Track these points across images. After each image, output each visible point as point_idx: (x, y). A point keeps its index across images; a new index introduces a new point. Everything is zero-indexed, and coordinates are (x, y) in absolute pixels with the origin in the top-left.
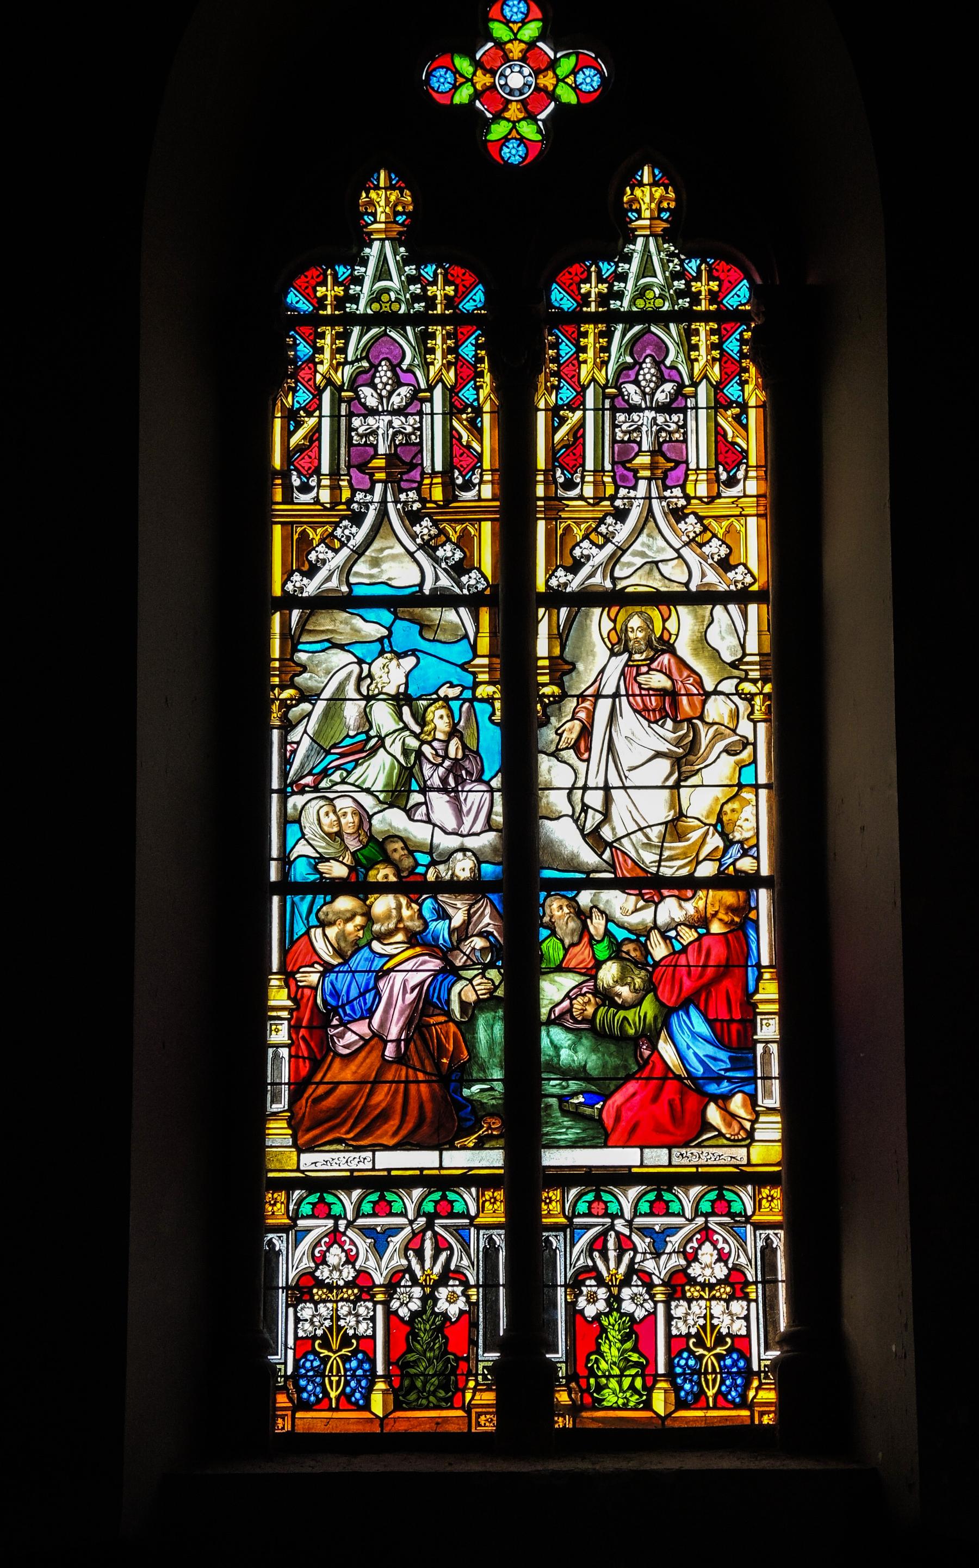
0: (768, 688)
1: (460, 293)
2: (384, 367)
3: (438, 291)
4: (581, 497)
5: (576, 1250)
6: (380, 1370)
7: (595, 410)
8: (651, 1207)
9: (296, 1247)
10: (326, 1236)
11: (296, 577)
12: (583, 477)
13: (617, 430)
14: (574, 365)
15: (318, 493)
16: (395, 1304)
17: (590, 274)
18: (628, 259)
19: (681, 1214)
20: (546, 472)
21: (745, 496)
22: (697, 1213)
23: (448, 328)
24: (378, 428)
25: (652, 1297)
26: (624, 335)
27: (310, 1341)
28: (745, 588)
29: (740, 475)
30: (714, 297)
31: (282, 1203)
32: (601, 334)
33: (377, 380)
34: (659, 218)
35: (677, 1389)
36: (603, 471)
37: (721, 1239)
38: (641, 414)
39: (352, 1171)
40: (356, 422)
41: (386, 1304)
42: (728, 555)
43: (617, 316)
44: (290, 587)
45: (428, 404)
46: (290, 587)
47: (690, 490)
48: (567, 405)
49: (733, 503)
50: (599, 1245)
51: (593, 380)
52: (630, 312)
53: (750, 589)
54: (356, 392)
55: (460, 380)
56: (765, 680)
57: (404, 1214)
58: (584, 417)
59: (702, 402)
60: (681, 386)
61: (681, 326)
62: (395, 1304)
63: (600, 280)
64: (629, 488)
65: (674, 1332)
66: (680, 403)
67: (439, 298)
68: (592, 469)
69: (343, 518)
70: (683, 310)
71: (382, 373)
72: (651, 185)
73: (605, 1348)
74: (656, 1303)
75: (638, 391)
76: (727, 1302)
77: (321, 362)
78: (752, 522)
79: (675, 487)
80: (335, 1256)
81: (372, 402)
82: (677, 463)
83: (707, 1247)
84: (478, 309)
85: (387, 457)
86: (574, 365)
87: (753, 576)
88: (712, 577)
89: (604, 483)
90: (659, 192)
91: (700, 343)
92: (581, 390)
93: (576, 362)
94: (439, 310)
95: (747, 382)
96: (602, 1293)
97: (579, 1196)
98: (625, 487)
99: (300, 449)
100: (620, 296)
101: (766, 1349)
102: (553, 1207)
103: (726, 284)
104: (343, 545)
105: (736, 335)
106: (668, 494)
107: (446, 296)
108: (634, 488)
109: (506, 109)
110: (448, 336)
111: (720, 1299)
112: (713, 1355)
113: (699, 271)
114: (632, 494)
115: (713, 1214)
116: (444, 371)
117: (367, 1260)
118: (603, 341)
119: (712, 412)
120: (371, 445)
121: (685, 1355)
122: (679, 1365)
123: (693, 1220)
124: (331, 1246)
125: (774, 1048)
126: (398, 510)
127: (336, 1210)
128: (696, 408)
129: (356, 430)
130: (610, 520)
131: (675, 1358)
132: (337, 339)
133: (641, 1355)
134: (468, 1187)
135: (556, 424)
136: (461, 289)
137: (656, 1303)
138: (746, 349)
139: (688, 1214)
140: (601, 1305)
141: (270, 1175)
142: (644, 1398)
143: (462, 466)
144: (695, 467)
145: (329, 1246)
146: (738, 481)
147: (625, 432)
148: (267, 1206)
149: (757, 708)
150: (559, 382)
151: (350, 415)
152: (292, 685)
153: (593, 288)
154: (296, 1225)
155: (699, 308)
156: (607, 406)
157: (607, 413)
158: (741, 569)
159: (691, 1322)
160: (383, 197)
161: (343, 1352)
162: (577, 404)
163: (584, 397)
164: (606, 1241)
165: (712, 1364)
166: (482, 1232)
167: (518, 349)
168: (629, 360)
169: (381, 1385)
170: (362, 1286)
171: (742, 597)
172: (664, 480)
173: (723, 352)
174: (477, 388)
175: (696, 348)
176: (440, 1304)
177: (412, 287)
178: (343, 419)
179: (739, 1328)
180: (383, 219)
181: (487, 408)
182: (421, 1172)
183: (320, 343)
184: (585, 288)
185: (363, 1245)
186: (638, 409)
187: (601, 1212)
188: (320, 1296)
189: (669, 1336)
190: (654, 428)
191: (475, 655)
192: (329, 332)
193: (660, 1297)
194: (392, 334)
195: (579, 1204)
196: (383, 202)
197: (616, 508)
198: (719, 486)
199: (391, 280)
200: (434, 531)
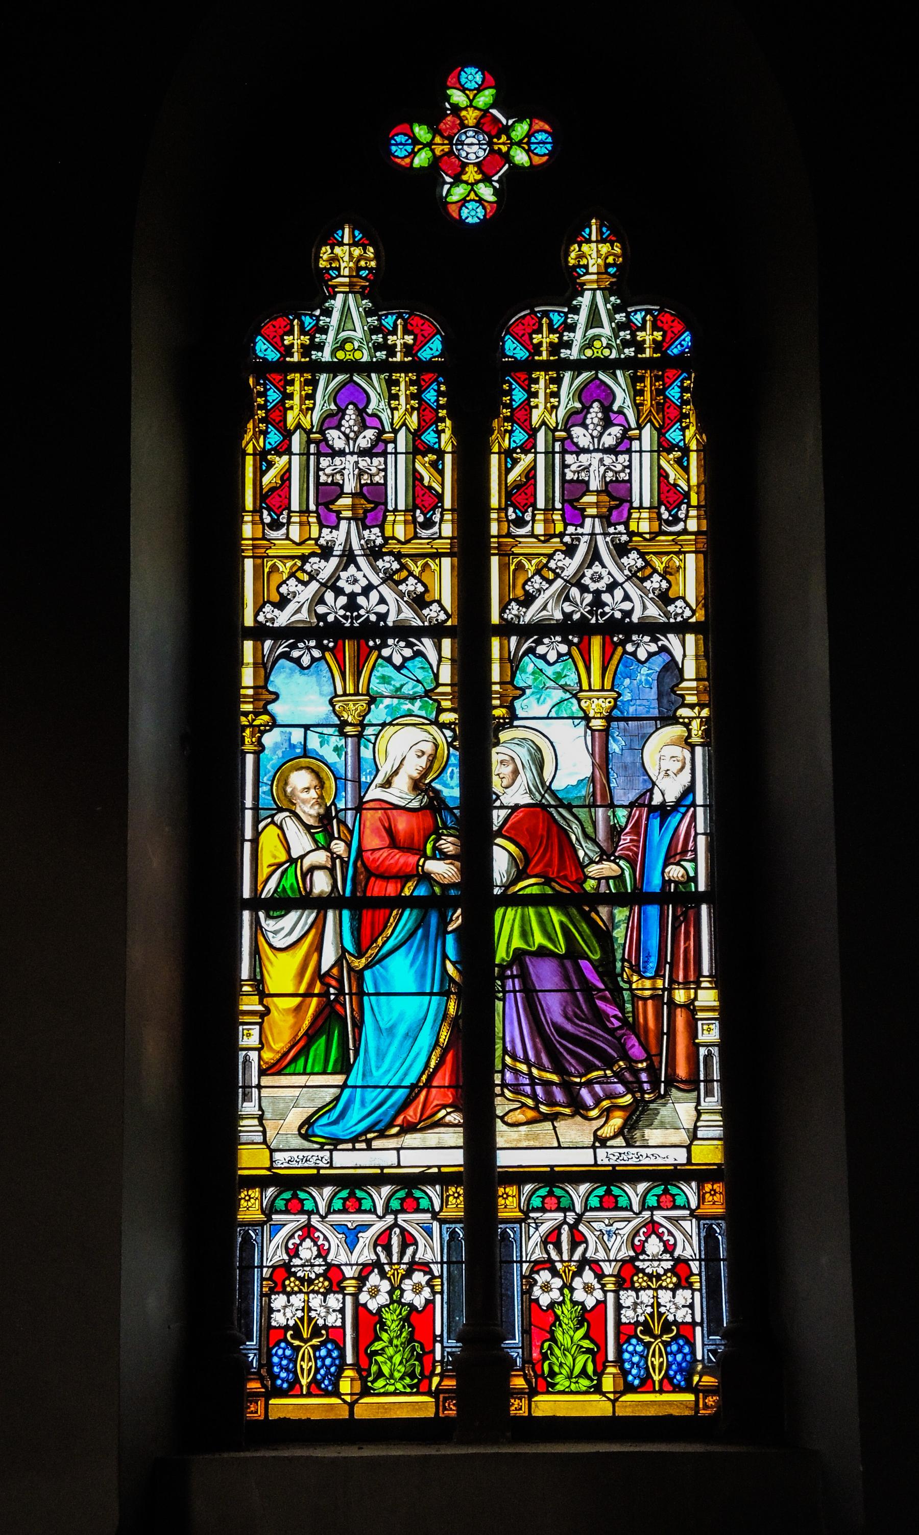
0: (705, 713)
1: (667, 340)
2: (351, 410)
3: (398, 340)
4: (533, 535)
5: (531, 1243)
6: (349, 1359)
7: (546, 453)
8: (601, 1202)
9: (270, 1241)
10: (644, 1226)
11: (268, 608)
12: (534, 516)
13: (321, 473)
14: (526, 410)
15: (533, 527)
16: (364, 1298)
17: (541, 325)
18: (576, 310)
19: (373, 1211)
20: (499, 510)
21: (440, 537)
22: (644, 1207)
23: (410, 375)
26: (573, 380)
27: (283, 1331)
28: (685, 621)
29: (437, 518)
30: (408, 350)
31: (721, 1193)
32: (307, 383)
33: (588, 421)
34: (358, 276)
35: (625, 1373)
36: (554, 509)
37: (322, 1237)
38: (343, 459)
39: (614, 1166)
40: (570, 459)
41: (355, 1296)
42: (668, 589)
43: (318, 367)
44: (261, 618)
45: (637, 442)
46: (261, 618)
47: (633, 526)
48: (520, 447)
49: (428, 544)
51: (544, 423)
52: (579, 361)
53: (690, 621)
54: (324, 435)
55: (423, 424)
56: (702, 706)
57: (373, 1211)
58: (535, 460)
59: (401, 447)
60: (382, 431)
61: (382, 376)
62: (364, 1298)
63: (303, 332)
64: (576, 526)
65: (624, 1320)
66: (381, 446)
67: (648, 342)
68: (404, 508)
69: (313, 554)
70: (628, 358)
71: (593, 415)
72: (350, 245)
73: (559, 1334)
75: (342, 436)
76: (325, 1295)
77: (291, 408)
78: (691, 559)
79: (619, 524)
80: (654, 1246)
81: (339, 444)
82: (377, 504)
83: (654, 1239)
84: (435, 357)
85: (353, 495)
86: (526, 410)
87: (446, 612)
88: (408, 613)
90: (605, 248)
91: (400, 393)
92: (288, 435)
93: (527, 407)
94: (648, 353)
96: (385, 1286)
97: (533, 1192)
98: (573, 525)
99: (518, 486)
100: (320, 347)
101: (449, 1338)
102: (509, 1203)
103: (670, 335)
104: (557, 576)
105: (678, 383)
106: (611, 530)
107: (405, 345)
108: (582, 526)
109: (463, 172)
110: (307, 383)
112: (311, 1346)
113: (644, 321)
114: (580, 530)
115: (659, 1208)
116: (407, 416)
117: (338, 1254)
118: (554, 388)
120: (338, 484)
121: (283, 1345)
122: (276, 1354)
123: (640, 1213)
124: (649, 1236)
125: (715, 1051)
126: (607, 542)
127: (309, 1205)
128: (396, 453)
129: (323, 470)
130: (559, 556)
131: (273, 1348)
132: (550, 383)
133: (592, 1341)
134: (433, 1185)
135: (264, 468)
137: (434, 1293)
138: (687, 396)
139: (636, 1208)
140: (555, 1295)
141: (240, 1172)
142: (595, 1382)
143: (668, 502)
144: (638, 505)
145: (302, 1239)
146: (434, 523)
148: (242, 1201)
149: (694, 732)
150: (512, 426)
151: (564, 452)
152: (266, 712)
153: (544, 339)
154: (271, 1220)
155: (395, 359)
156: (557, 449)
158: (435, 607)
159: (289, 1315)
160: (595, 250)
161: (665, 1338)
163: (535, 439)
164: (560, 1234)
165: (659, 1348)
166: (445, 1227)
167: (474, 395)
168: (578, 405)
169: (349, 1373)
170: (333, 1278)
171: (436, 632)
172: (363, 520)
173: (421, 401)
174: (439, 433)
175: (396, 397)
176: (406, 1294)
177: (622, 334)
178: (557, 456)
179: (333, 1320)
180: (346, 272)
181: (693, 446)
182: (382, 1171)
183: (534, 388)
184: (537, 338)
185: (335, 1241)
186: (342, 453)
187: (670, 1205)
188: (292, 1289)
189: (618, 1323)
191: (438, 685)
192: (542, 376)
196: (346, 255)
197: (565, 544)
198: (415, 528)
199: (603, 327)
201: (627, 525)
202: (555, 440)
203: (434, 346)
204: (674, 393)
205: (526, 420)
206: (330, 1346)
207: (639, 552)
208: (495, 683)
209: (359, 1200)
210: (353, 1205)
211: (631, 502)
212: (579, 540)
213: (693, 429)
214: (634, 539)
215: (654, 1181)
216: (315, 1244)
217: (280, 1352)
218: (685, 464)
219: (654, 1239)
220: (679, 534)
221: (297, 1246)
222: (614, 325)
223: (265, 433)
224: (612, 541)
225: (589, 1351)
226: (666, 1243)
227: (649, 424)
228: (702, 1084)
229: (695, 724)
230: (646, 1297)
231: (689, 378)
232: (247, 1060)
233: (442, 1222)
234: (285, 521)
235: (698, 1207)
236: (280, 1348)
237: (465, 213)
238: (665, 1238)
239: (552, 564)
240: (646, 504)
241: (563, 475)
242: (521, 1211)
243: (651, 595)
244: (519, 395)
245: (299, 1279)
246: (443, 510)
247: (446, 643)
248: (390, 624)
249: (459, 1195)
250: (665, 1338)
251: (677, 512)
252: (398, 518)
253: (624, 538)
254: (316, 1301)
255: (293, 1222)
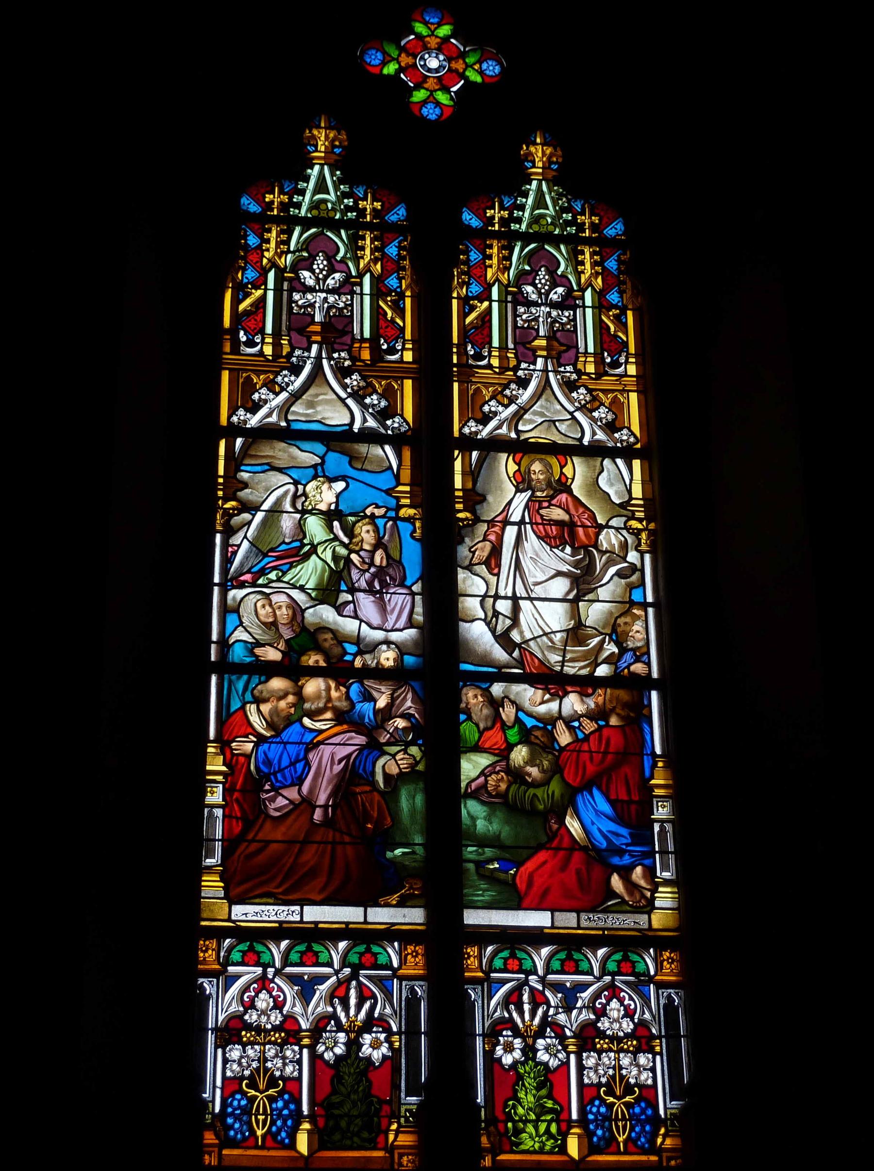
0: (652, 526)
4: (489, 366)
11: (241, 412)
15: (626, 368)
16: (321, 1048)
18: (526, 195)
19: (590, 972)
21: (626, 375)
22: (604, 972)
24: (315, 302)
25: (565, 1048)
29: (622, 360)
30: (594, 227)
32: (503, 248)
33: (537, 281)
36: (507, 348)
37: (627, 997)
40: (296, 296)
44: (235, 419)
47: (580, 366)
49: (616, 380)
50: (514, 998)
51: (497, 280)
52: (526, 233)
57: (590, 972)
64: (529, 363)
65: (586, 1081)
70: (569, 234)
73: (521, 1095)
74: (568, 1054)
80: (263, 1001)
81: (310, 282)
82: (569, 348)
83: (614, 1004)
87: (635, 437)
88: (601, 436)
89: (508, 358)
92: (264, 272)
95: (625, 292)
97: (494, 954)
100: (519, 221)
102: (474, 960)
107: (374, 210)
108: (535, 363)
111: (627, 1051)
115: (619, 973)
117: (293, 1005)
119: (597, 311)
120: (309, 314)
121: (597, 1103)
122: (591, 1112)
125: (668, 827)
126: (558, 379)
129: (297, 302)
133: (556, 1102)
135: (241, 297)
136: (387, 205)
139: (596, 972)
140: (517, 1054)
147: (525, 321)
149: (643, 541)
150: (469, 279)
154: (226, 971)
156: (285, 287)
157: (509, 305)
160: (540, 151)
161: (627, 1099)
162: (485, 296)
164: (348, 990)
165: (622, 1111)
170: (289, 1032)
173: (384, 255)
175: (582, 263)
185: (289, 991)
187: (516, 968)
188: (629, 1047)
190: (326, 305)
193: (572, 1048)
194: (329, 234)
195: (350, 955)
199: (329, 193)
200: (362, 384)
201: (575, 365)
202: (508, 293)
203: (400, 213)
204: (392, 250)
205: (481, 276)
206: (286, 1097)
207: (587, 388)
208: (221, 477)
209: (577, 962)
210: (571, 966)
211: (578, 349)
212: (305, 362)
213: (629, 293)
214: (583, 377)
215: (295, 940)
216: (622, 1004)
217: (594, 1110)
218: (624, 320)
219: (263, 995)
220: (621, 376)
221: (604, 1006)
222: (338, 193)
223: (468, 284)
224: (562, 378)
225: (551, 1111)
226: (275, 999)
227: (590, 288)
228: (657, 856)
229: (644, 536)
230: (608, 1059)
231: (625, 254)
232: (211, 814)
233: (401, 979)
234: (486, 354)
235: (400, 968)
236: (594, 1106)
237: (425, 111)
238: (626, 1002)
239: (508, 392)
240: (591, 349)
241: (515, 322)
242: (219, 963)
243: (599, 423)
244: (475, 256)
245: (609, 1037)
246: (405, 340)
247: (637, 464)
248: (586, 443)
249: (417, 954)
250: (627, 1099)
251: (394, 345)
252: (588, 359)
253: (574, 376)
254: (625, 1061)
255: (250, 973)
